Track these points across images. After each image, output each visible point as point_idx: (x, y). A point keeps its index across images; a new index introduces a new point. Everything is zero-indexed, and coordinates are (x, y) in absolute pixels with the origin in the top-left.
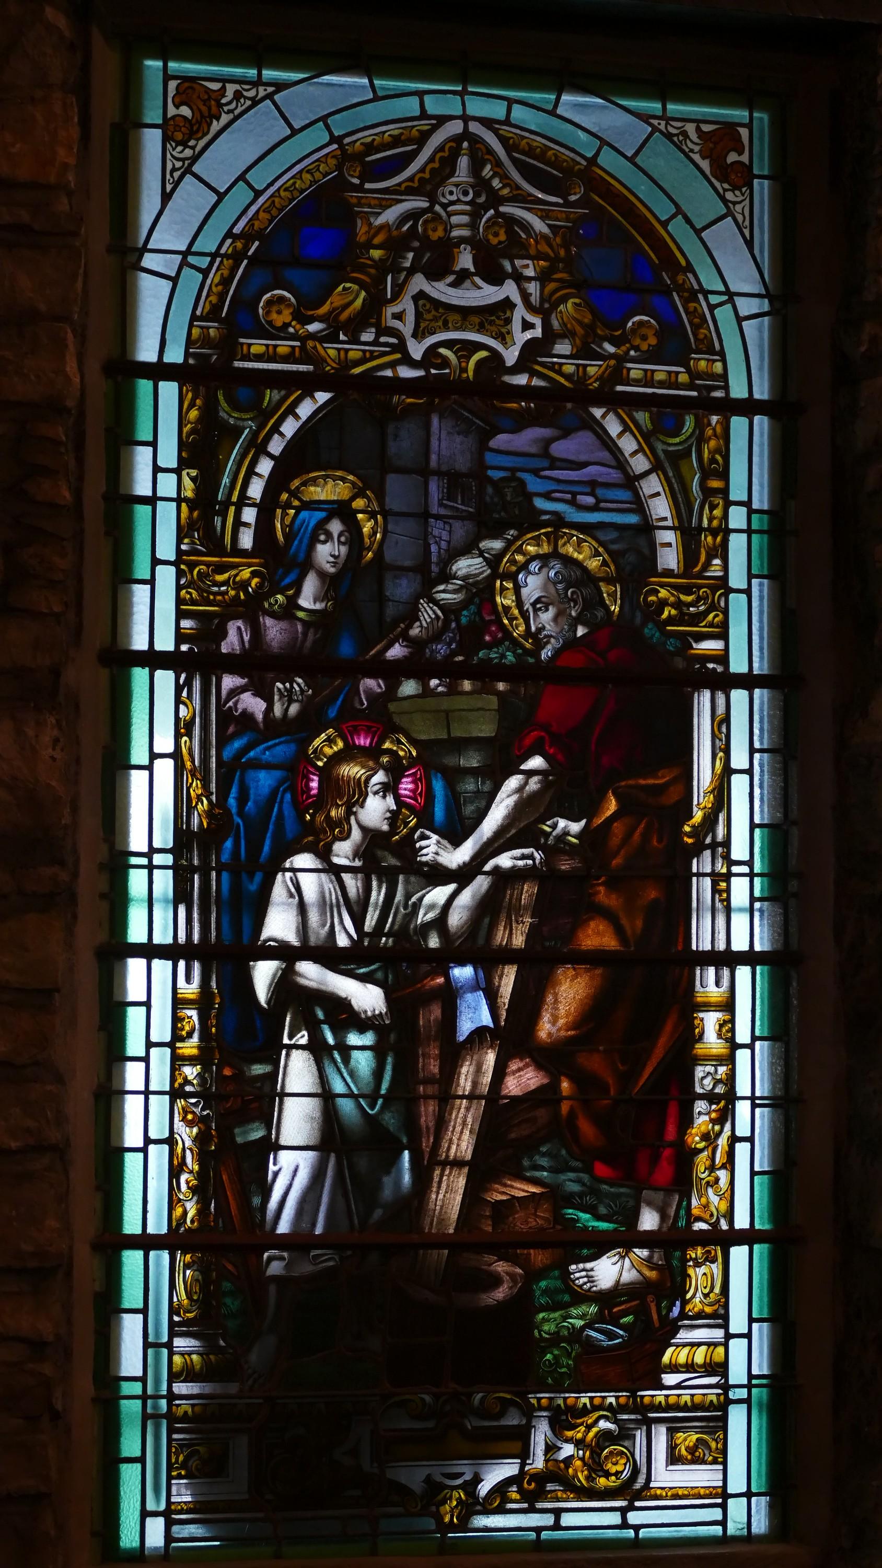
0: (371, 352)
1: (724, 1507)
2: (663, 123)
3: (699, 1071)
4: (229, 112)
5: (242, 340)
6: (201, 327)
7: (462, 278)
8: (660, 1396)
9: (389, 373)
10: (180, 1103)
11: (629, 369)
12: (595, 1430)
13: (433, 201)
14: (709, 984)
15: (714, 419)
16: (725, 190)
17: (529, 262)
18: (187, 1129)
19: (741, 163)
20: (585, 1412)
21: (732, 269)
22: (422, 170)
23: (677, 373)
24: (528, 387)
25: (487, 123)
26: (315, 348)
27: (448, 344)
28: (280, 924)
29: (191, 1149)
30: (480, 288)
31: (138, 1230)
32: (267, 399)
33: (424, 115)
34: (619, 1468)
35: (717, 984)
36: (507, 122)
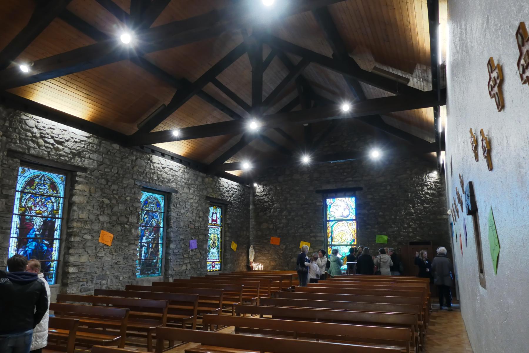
21: (162, 204)
28: (143, 241)
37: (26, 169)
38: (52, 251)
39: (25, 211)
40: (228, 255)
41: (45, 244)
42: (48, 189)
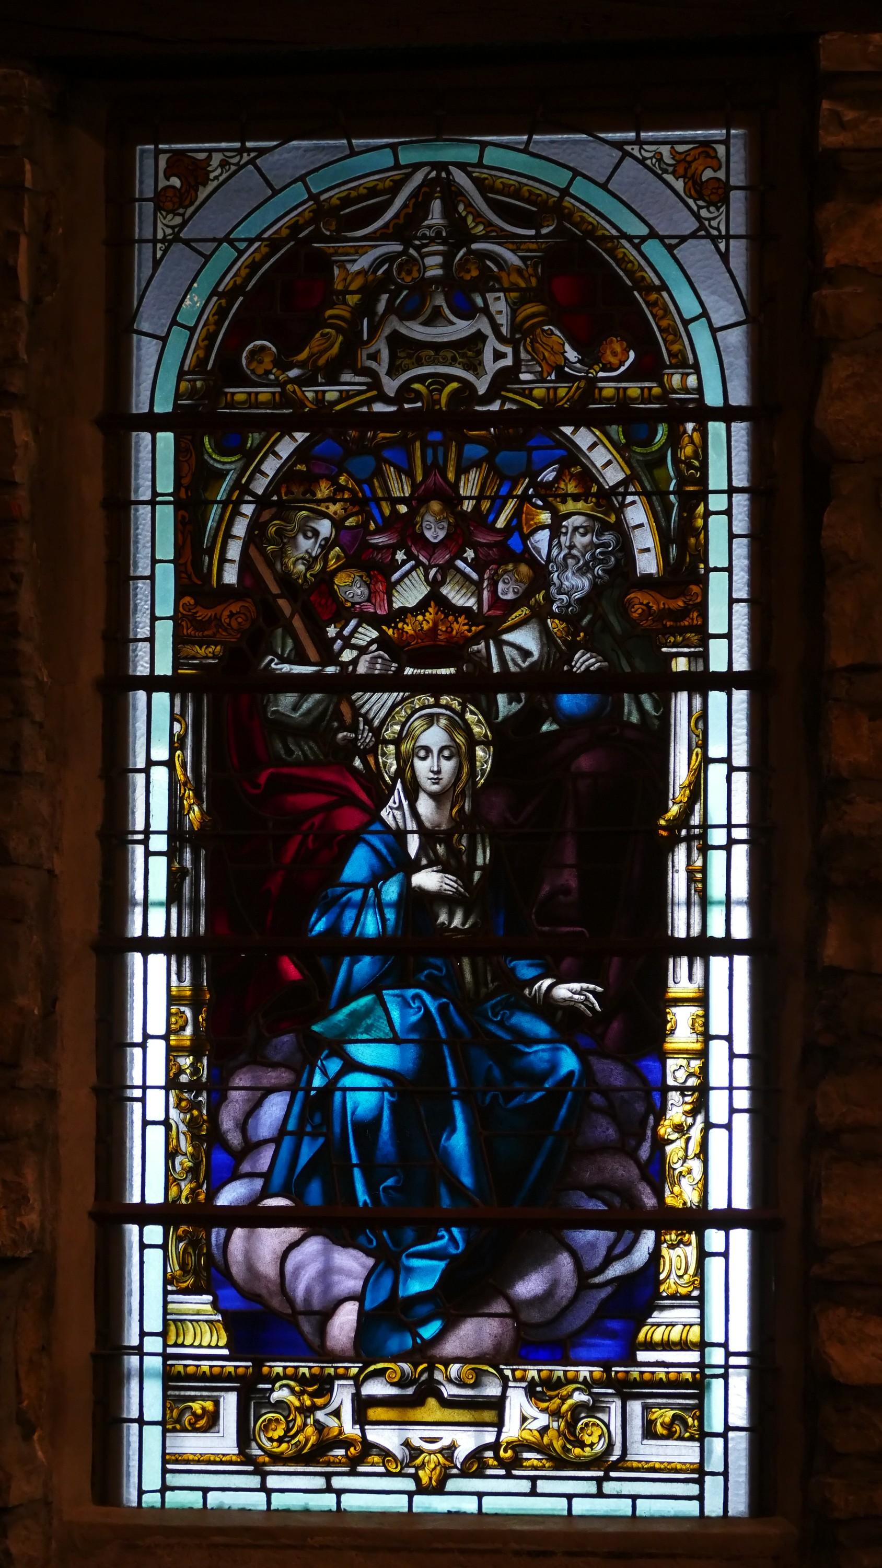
0: (348, 391)
1: (700, 1482)
2: (636, 148)
3: (671, 1064)
4: (216, 178)
5: (227, 390)
6: (189, 381)
7: (435, 318)
8: (635, 1372)
9: (365, 409)
10: (172, 1094)
11: (601, 389)
12: (570, 1402)
13: (407, 243)
14: (681, 979)
15: (690, 426)
16: (700, 207)
17: (502, 294)
18: (182, 1115)
19: (718, 180)
20: (560, 1384)
22: (397, 216)
23: (650, 389)
24: (501, 412)
25: (462, 166)
26: (294, 392)
27: (421, 379)
29: (184, 1133)
30: (452, 323)
31: (723, 668)
32: (250, 442)
33: (397, 166)
34: (595, 1439)
35: (690, 978)
36: (480, 164)
37: (214, 151)
38: (655, 1096)
39: (257, 641)
40: (685, 643)
41: (547, 1008)
42: (519, 335)
